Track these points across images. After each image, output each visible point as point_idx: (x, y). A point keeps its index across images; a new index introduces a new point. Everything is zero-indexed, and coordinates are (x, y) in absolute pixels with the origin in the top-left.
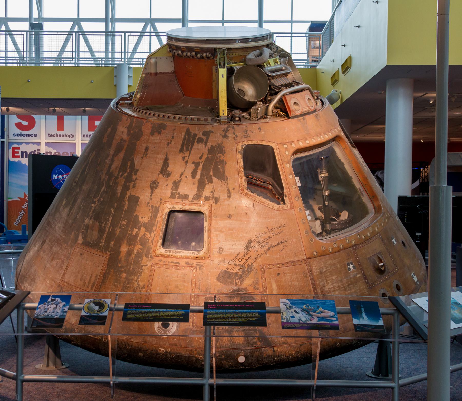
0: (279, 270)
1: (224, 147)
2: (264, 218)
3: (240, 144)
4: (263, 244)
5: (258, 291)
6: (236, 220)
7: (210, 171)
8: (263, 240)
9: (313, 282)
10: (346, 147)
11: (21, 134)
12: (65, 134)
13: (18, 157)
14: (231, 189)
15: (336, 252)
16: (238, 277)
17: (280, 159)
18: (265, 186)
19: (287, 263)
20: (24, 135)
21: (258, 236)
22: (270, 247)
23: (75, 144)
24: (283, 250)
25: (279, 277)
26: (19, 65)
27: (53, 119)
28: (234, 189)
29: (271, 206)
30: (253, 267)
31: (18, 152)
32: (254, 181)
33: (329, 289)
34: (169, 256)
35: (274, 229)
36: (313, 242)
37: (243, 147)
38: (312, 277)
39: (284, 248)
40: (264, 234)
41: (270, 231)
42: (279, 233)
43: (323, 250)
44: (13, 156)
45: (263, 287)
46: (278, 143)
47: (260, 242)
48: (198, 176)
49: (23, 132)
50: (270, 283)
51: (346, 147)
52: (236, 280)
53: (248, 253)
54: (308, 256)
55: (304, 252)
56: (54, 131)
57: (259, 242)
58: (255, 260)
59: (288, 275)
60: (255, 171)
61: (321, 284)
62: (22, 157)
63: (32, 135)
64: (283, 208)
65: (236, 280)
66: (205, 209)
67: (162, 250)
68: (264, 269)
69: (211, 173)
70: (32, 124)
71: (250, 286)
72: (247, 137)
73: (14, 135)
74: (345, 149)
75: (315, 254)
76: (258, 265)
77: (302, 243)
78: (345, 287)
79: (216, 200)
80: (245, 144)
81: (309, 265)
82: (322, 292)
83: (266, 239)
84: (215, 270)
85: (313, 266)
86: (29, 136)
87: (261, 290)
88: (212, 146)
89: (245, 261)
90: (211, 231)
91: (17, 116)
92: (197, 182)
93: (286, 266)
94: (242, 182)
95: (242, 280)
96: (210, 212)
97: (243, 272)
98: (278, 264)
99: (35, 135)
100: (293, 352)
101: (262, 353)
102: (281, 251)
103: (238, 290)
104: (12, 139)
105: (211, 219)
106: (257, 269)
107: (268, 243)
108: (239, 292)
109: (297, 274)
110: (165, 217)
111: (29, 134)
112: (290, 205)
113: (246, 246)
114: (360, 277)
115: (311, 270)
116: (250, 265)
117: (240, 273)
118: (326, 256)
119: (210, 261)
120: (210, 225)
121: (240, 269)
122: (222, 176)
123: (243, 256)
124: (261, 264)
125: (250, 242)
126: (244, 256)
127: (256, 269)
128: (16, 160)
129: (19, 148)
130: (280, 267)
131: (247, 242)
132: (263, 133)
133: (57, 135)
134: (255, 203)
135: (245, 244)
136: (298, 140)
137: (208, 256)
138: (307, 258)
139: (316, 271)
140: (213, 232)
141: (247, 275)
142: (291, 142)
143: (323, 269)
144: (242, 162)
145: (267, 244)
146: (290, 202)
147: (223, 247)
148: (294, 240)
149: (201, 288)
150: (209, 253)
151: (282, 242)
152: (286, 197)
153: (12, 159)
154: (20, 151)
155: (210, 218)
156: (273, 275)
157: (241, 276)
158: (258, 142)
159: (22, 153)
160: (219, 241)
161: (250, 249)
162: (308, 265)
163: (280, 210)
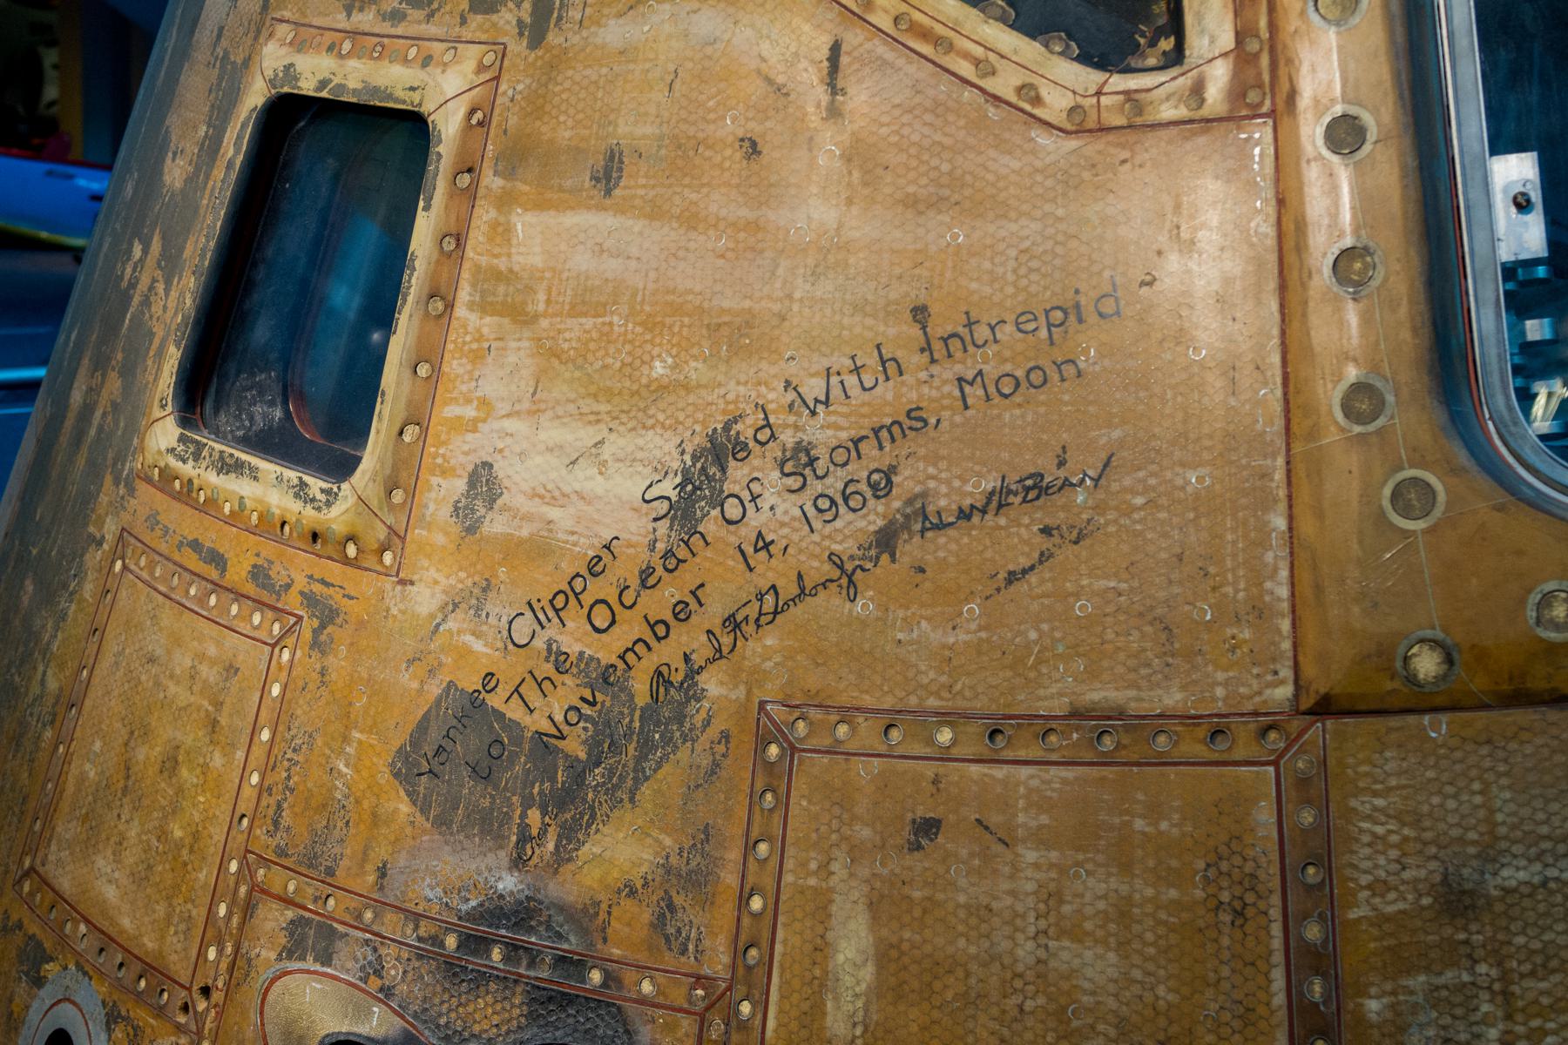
0: (936, 781)
2: (911, 203)
4: (834, 485)
6: (655, 212)
8: (844, 435)
16: (553, 779)
19: (1045, 727)
21: (813, 388)
22: (906, 527)
24: (1033, 578)
25: (918, 862)
29: (1005, 84)
34: (186, 493)
35: (982, 333)
36: (1420, 525)
38: (1313, 932)
39: (1044, 557)
40: (868, 381)
41: (937, 346)
42: (1036, 377)
43: (1552, 636)
45: (743, 939)
47: (812, 462)
50: (821, 908)
52: (527, 804)
53: (682, 553)
55: (1286, 625)
57: (800, 462)
58: (726, 640)
59: (1031, 856)
64: (1139, 109)
65: (527, 804)
68: (791, 749)
71: (633, 893)
75: (1427, 664)
76: (741, 692)
77: (1280, 523)
83: (876, 431)
84: (408, 680)
87: (718, 962)
89: (639, 630)
90: (450, 306)
93: (1022, 754)
95: (576, 820)
96: (479, 121)
97: (604, 742)
98: (947, 717)
102: (1012, 578)
103: (522, 914)
105: (471, 194)
106: (725, 737)
107: (889, 473)
108: (531, 930)
109: (1126, 868)
110: (237, 152)
112: (1236, 74)
113: (682, 486)
116: (677, 678)
117: (575, 746)
120: (449, 245)
121: (586, 710)
123: (634, 582)
124: (770, 690)
126: (643, 584)
127: (713, 732)
130: (955, 752)
134: (854, 38)
135: (676, 465)
137: (382, 533)
138: (1306, 703)
140: (460, 311)
141: (630, 783)
143: (1490, 856)
145: (883, 484)
146: (1240, 37)
147: (501, 469)
149: (287, 818)
150: (392, 508)
151: (1037, 488)
155: (465, 180)
156: (866, 833)
157: (578, 773)
160: (484, 403)
161: (711, 525)
162: (1303, 782)
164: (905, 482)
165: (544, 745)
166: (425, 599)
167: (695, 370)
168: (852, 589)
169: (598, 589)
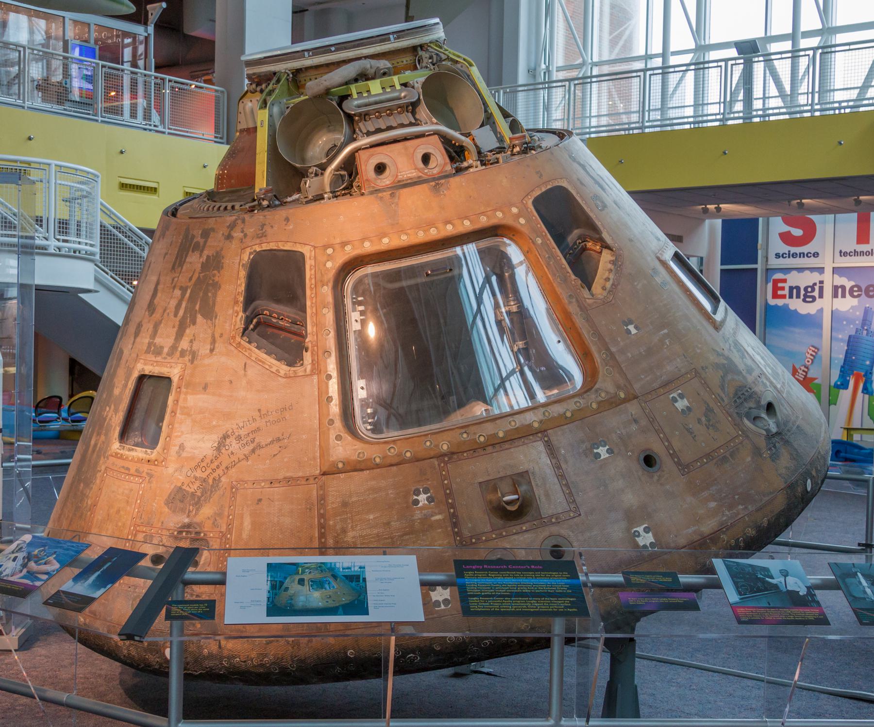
1: (223, 257)
3: (248, 250)
4: (244, 442)
5: (218, 529)
7: (196, 304)
9: (322, 521)
10: (529, 249)
11: (789, 254)
12: (789, 251)
13: (784, 297)
14: (217, 335)
15: (392, 465)
17: (313, 277)
18: (295, 330)
20: (794, 255)
21: (241, 425)
23: (756, 269)
26: (692, 126)
27: (849, 222)
28: (221, 335)
30: (221, 485)
31: (783, 288)
32: (274, 320)
33: (353, 537)
35: (270, 413)
37: (251, 257)
38: (322, 511)
39: (280, 452)
44: (775, 296)
46: (316, 245)
48: (181, 313)
49: (794, 250)
51: (529, 249)
54: (324, 469)
56: (851, 244)
57: (239, 438)
59: (277, 503)
60: (278, 301)
61: (338, 527)
62: (791, 297)
63: (809, 255)
64: (296, 373)
66: (175, 373)
67: (116, 445)
69: (197, 307)
70: (810, 233)
72: (262, 237)
73: (778, 256)
74: (528, 252)
78: (392, 538)
79: (194, 356)
80: (255, 251)
81: (322, 487)
85: (330, 489)
86: (804, 257)
87: (224, 529)
88: (208, 257)
90: (175, 414)
91: (782, 219)
92: (177, 324)
94: (236, 322)
96: (181, 378)
99: (816, 255)
100: (254, 655)
101: (200, 648)
102: (274, 456)
103: (189, 526)
104: (774, 263)
105: (180, 393)
111: (804, 254)
115: (322, 498)
117: (199, 494)
119: (163, 468)
120: (176, 402)
122: (209, 313)
125: (225, 437)
127: (224, 487)
128: (780, 302)
129: (785, 281)
131: (222, 436)
132: (291, 227)
133: (856, 253)
134: (249, 362)
136: (363, 240)
140: (178, 415)
142: (344, 244)
144: (244, 285)
145: (253, 441)
151: (278, 440)
152: (306, 351)
153: (772, 302)
154: (786, 286)
155: (178, 390)
157: (199, 498)
158: (278, 246)
159: (791, 289)
161: (223, 451)
164: (257, 440)
165: (193, 494)
169: (204, 464)
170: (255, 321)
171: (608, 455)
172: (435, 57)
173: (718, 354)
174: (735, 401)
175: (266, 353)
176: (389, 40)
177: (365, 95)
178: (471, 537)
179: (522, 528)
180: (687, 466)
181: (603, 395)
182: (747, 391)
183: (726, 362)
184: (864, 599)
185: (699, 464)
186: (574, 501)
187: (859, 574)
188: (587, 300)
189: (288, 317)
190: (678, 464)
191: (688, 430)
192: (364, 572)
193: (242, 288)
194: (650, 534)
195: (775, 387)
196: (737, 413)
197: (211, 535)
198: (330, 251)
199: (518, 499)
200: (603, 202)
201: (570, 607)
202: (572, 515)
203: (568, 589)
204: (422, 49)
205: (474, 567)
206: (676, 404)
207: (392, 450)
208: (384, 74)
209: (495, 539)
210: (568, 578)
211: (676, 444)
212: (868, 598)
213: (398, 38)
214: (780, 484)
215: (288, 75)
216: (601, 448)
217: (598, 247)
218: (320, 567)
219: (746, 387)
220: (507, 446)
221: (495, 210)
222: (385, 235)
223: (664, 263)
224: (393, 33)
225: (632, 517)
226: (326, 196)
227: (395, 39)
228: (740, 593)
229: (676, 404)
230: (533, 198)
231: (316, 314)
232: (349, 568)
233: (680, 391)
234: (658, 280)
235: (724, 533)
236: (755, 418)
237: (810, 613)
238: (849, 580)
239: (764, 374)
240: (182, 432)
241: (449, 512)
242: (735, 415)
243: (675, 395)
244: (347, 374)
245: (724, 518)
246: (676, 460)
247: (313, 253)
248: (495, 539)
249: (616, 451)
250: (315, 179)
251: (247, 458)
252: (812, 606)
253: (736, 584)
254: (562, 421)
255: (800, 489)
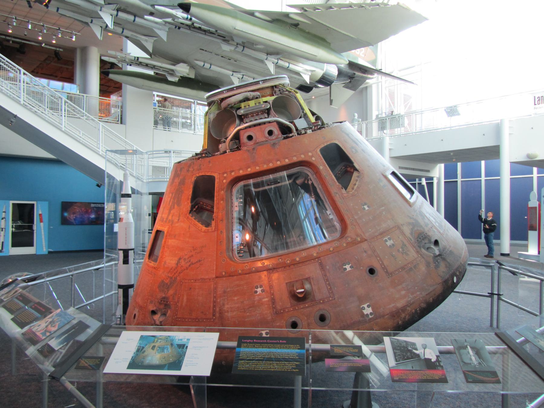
3: (194, 176)
4: (186, 261)
15: (246, 274)
32: (205, 207)
33: (228, 308)
38: (215, 295)
59: (197, 290)
60: (206, 198)
61: (221, 303)
75: (224, 273)
82: (220, 310)
87: (176, 301)
88: (181, 179)
96: (168, 232)
98: (192, 279)
103: (164, 298)
114: (267, 301)
115: (216, 288)
117: (169, 284)
118: (234, 277)
136: (239, 170)
139: (220, 291)
140: (165, 248)
144: (191, 191)
146: (215, 225)
148: (210, 260)
151: (200, 261)
152: (213, 220)
161: (179, 265)
163: (206, 232)
164: (191, 261)
165: (167, 284)
166: (161, 272)
167: (179, 252)
168: (187, 269)
169: (172, 271)
170: (196, 207)
171: (350, 269)
172: (281, 90)
173: (411, 218)
174: (418, 240)
175: (197, 221)
176: (260, 84)
177: (247, 107)
178: (281, 310)
179: (305, 305)
180: (391, 274)
181: (349, 239)
182: (424, 235)
183: (414, 222)
184: (470, 364)
185: (397, 272)
186: (332, 292)
187: (468, 347)
188: (344, 195)
189: (210, 205)
190: (387, 272)
191: (392, 255)
192: (188, 342)
193: (191, 193)
194: (370, 308)
195: (440, 232)
196: (418, 246)
197: (172, 303)
198: (225, 175)
199: (304, 291)
200: (356, 150)
201: (295, 369)
202: (331, 299)
203: (297, 356)
204: (276, 88)
205: (248, 341)
206: (387, 243)
207: (247, 267)
208: (257, 98)
209: (292, 311)
210: (299, 349)
211: (386, 263)
212: (473, 363)
213: (264, 83)
214: (439, 280)
215: (218, 101)
216: (347, 265)
217: (352, 170)
218: (167, 338)
219: (423, 233)
220: (300, 265)
221: (301, 154)
222: (249, 167)
223: (386, 177)
224: (262, 81)
225: (361, 300)
226: (227, 151)
227: (262, 83)
228: (396, 360)
229: (387, 243)
230: (320, 149)
231: (218, 204)
232: (181, 340)
233: (389, 237)
234: (382, 184)
235: (409, 306)
236: (428, 248)
237: (436, 374)
238: (462, 351)
239: (434, 226)
240: (166, 256)
241: (271, 297)
242: (417, 247)
243: (386, 238)
244: (231, 230)
245: (409, 299)
246: (385, 270)
247: (219, 176)
248: (292, 311)
249: (354, 267)
250: (223, 144)
251: (187, 269)
252: (438, 369)
253: (395, 354)
254: (328, 253)
255: (450, 282)
